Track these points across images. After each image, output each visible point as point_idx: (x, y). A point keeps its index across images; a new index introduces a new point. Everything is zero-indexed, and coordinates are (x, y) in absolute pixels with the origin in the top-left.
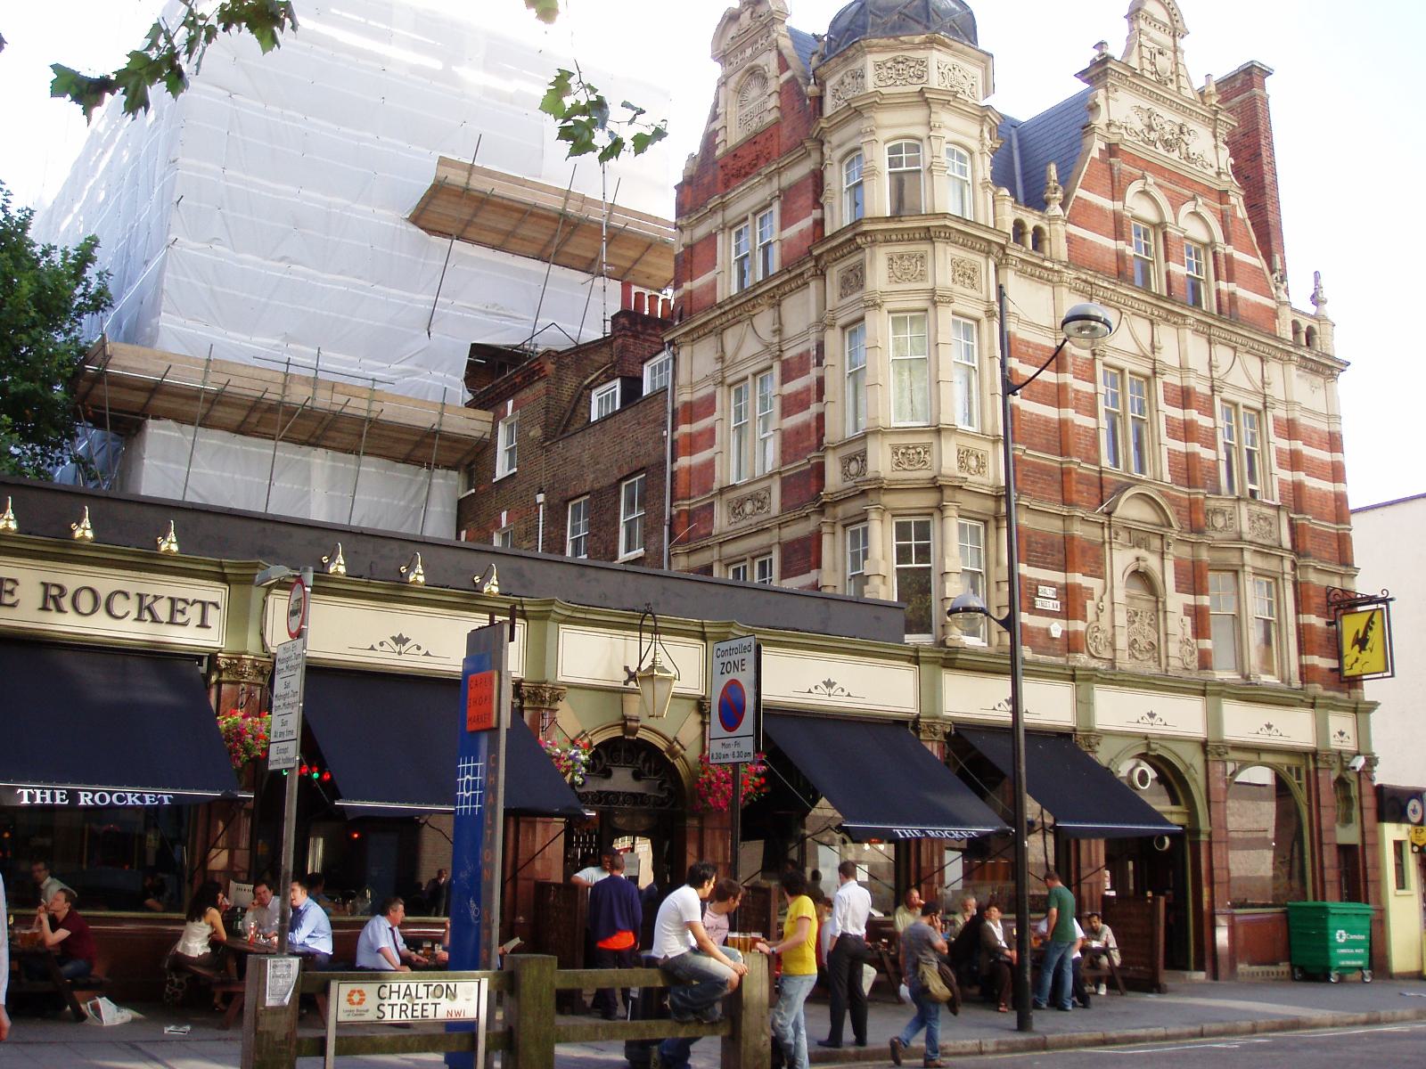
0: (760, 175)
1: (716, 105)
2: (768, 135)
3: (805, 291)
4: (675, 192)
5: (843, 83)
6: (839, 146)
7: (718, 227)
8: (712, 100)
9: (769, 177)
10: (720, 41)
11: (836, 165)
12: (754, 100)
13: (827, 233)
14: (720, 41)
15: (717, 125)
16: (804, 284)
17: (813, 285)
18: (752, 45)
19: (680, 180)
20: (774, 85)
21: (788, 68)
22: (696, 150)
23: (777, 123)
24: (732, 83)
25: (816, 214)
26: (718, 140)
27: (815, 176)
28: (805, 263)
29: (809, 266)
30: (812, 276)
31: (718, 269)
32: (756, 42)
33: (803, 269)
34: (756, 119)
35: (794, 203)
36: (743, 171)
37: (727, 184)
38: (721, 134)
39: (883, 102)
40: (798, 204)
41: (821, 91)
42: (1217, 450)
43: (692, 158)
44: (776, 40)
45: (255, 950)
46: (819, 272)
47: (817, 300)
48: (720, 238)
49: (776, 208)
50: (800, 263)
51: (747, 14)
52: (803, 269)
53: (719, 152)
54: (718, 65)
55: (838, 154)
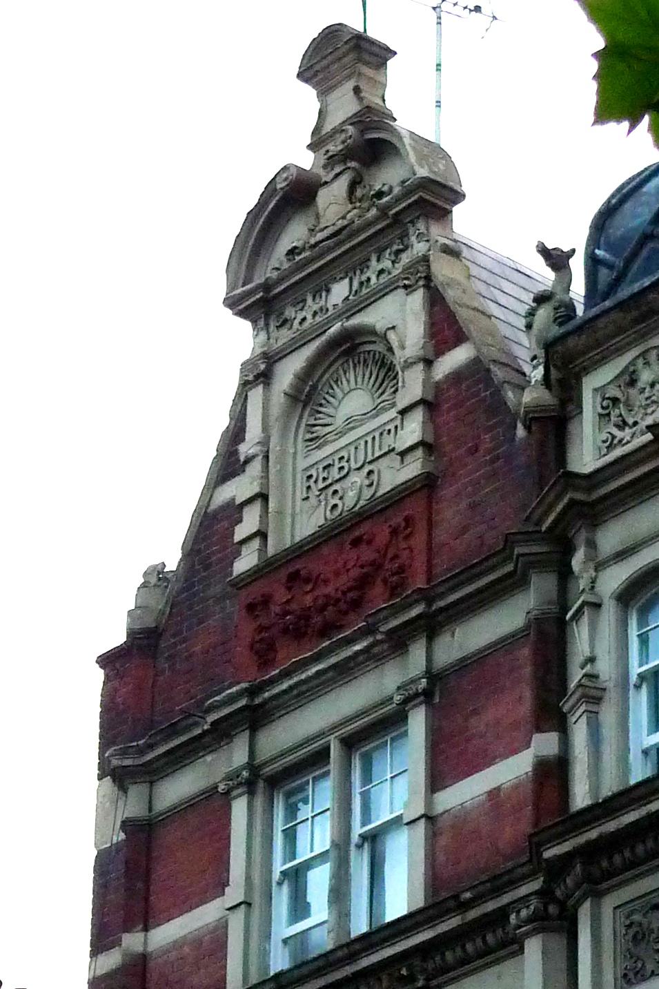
0: (369, 630)
1: (236, 433)
2: (398, 520)
3: (508, 967)
4: (99, 675)
5: (632, 382)
6: (622, 555)
7: (236, 774)
8: (222, 421)
9: (398, 643)
10: (251, 268)
11: (610, 612)
12: (351, 423)
13: (581, 798)
14: (251, 268)
15: (240, 488)
16: (503, 944)
17: (533, 948)
18: (349, 273)
19: (118, 638)
20: (413, 386)
21: (459, 337)
22: (172, 560)
23: (426, 485)
24: (287, 372)
25: (545, 744)
26: (241, 532)
27: (542, 635)
28: (514, 883)
29: (524, 890)
30: (529, 920)
31: (234, 893)
32: (364, 264)
33: (506, 899)
34: (358, 479)
35: (475, 712)
36: (317, 620)
37: (264, 654)
38: (249, 523)
39: (596, 495)
40: (489, 715)
41: (563, 403)
42: (369, 788)
43: (157, 577)
44: (425, 259)
45: (357, 373)
46: (553, 909)
47: (332, 827)
48: (239, 808)
49: (418, 722)
50: (500, 883)
51: (340, 187)
52: (506, 899)
53: (246, 562)
54: (246, 326)
55: (615, 578)
